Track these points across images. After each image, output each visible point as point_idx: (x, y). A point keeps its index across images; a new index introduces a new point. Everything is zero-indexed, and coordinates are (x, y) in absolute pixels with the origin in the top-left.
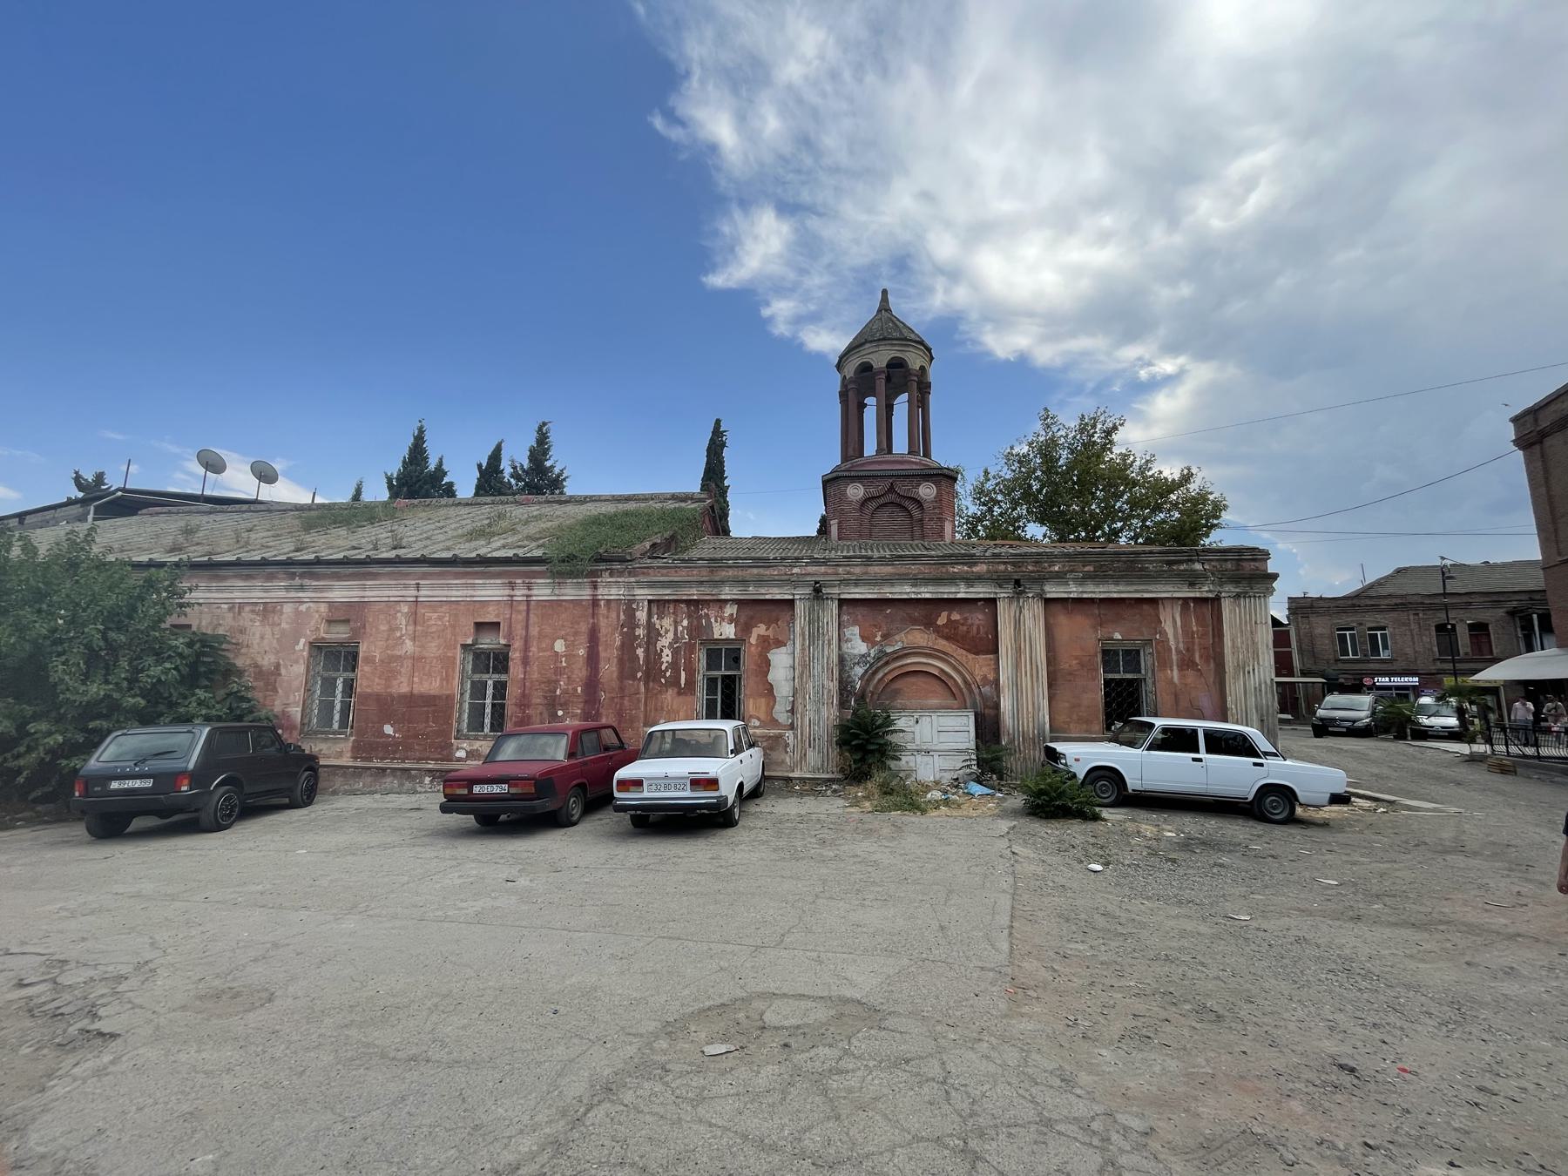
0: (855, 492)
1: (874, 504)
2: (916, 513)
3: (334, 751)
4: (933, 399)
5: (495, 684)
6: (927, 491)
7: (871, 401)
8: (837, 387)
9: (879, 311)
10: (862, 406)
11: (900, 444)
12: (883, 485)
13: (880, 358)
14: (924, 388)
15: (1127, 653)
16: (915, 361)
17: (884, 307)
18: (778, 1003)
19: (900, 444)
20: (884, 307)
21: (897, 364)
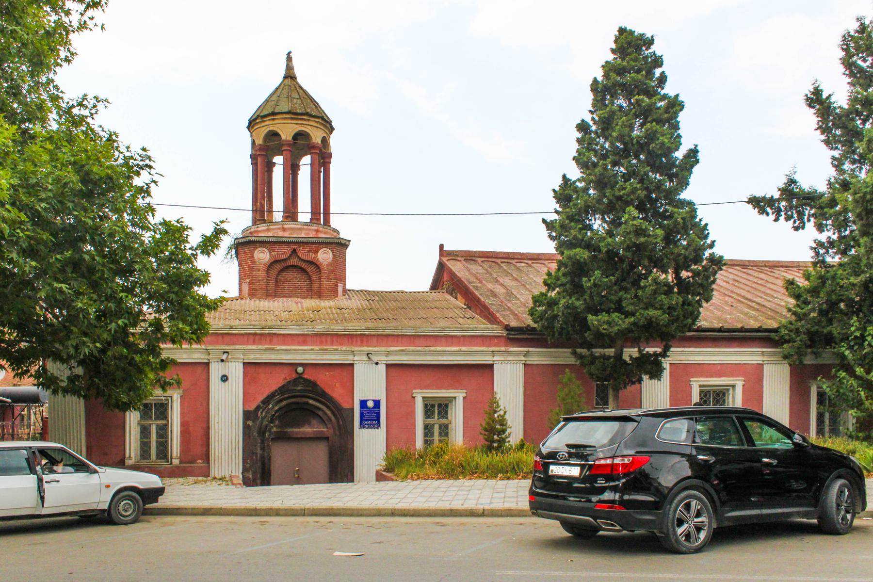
0: (263, 256)
1: (278, 267)
2: (314, 277)
3: (822, 338)
4: (333, 167)
5: (429, 408)
6: (324, 256)
7: (278, 160)
8: (249, 150)
9: (285, 77)
10: (270, 166)
11: (304, 212)
12: (286, 251)
13: (287, 130)
14: (323, 159)
15: (440, 405)
16: (316, 137)
17: (290, 76)
18: (286, 110)
19: (304, 212)
20: (290, 76)
21: (300, 136)
